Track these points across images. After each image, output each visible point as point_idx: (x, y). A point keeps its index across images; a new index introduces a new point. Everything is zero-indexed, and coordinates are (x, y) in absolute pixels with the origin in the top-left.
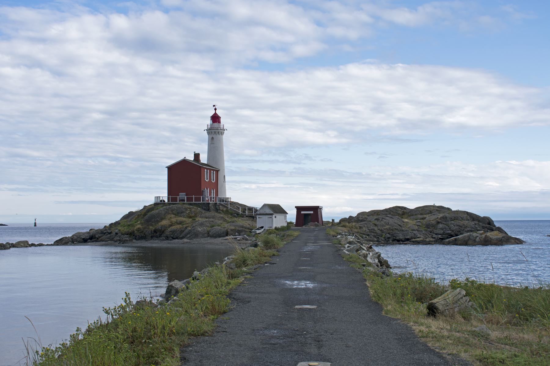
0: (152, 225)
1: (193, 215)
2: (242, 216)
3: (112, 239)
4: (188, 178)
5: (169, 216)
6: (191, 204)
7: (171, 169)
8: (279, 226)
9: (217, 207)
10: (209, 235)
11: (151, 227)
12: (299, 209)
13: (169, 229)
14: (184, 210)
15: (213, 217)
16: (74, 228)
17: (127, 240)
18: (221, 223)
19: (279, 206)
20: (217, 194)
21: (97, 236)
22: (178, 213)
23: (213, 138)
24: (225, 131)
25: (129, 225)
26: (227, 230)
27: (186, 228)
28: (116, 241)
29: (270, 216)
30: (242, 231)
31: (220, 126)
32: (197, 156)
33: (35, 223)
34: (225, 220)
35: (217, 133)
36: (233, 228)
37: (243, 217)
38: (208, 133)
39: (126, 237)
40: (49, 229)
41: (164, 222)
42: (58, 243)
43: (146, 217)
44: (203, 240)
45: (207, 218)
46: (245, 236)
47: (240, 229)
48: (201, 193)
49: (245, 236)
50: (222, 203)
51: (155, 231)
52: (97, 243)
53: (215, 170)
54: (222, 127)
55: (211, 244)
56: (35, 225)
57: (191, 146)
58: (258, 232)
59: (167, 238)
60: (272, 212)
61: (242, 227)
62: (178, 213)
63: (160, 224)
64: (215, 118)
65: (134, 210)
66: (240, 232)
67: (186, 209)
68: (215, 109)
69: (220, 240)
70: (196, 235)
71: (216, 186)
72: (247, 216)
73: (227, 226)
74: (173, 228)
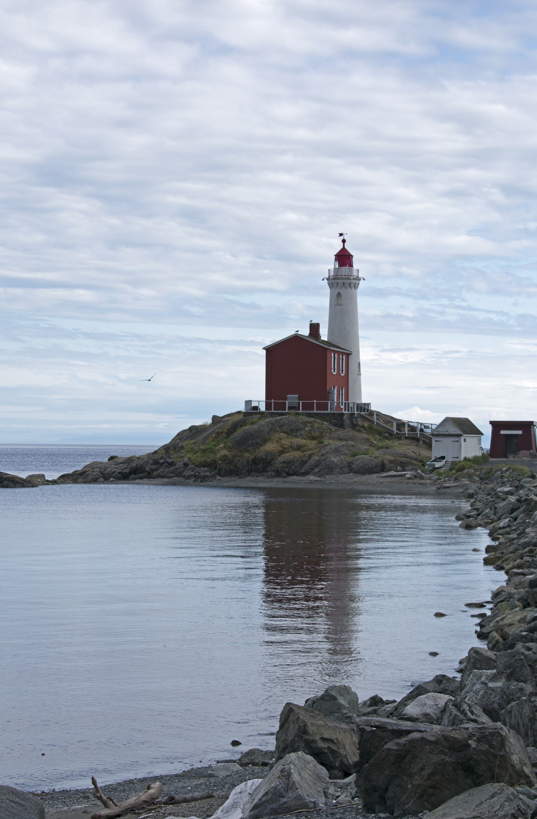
0: (248, 451)
1: (317, 434)
2: (399, 437)
3: (179, 475)
4: (305, 367)
5: (277, 436)
6: (310, 415)
8: (470, 455)
9: (354, 420)
10: (350, 469)
11: (246, 454)
12: (497, 426)
13: (281, 459)
14: (301, 426)
15: (352, 439)
16: (87, 455)
17: (208, 476)
18: (367, 450)
19: (467, 420)
20: (347, 399)
21: (147, 469)
22: (292, 431)
23: (339, 294)
24: (362, 282)
25: (204, 451)
26: (382, 461)
27: (310, 456)
28: (187, 478)
29: (456, 439)
30: (407, 464)
31: (351, 271)
32: (314, 328)
34: (372, 445)
35: (347, 285)
37: (399, 439)
38: (331, 285)
39: (204, 471)
40: (52, 455)
41: (270, 447)
42: (64, 479)
44: (342, 478)
45: (341, 440)
46: (419, 471)
47: (405, 460)
48: (326, 395)
49: (419, 471)
50: (363, 413)
51: (255, 461)
53: (347, 355)
54: (355, 274)
55: (362, 484)
57: (305, 311)
58: (437, 465)
59: (278, 474)
60: (459, 432)
61: (406, 456)
62: (293, 432)
63: (262, 448)
64: (344, 258)
65: (198, 422)
66: (404, 466)
67: (305, 424)
68: (344, 241)
70: (330, 469)
71: (346, 382)
72: (406, 438)
74: (287, 456)
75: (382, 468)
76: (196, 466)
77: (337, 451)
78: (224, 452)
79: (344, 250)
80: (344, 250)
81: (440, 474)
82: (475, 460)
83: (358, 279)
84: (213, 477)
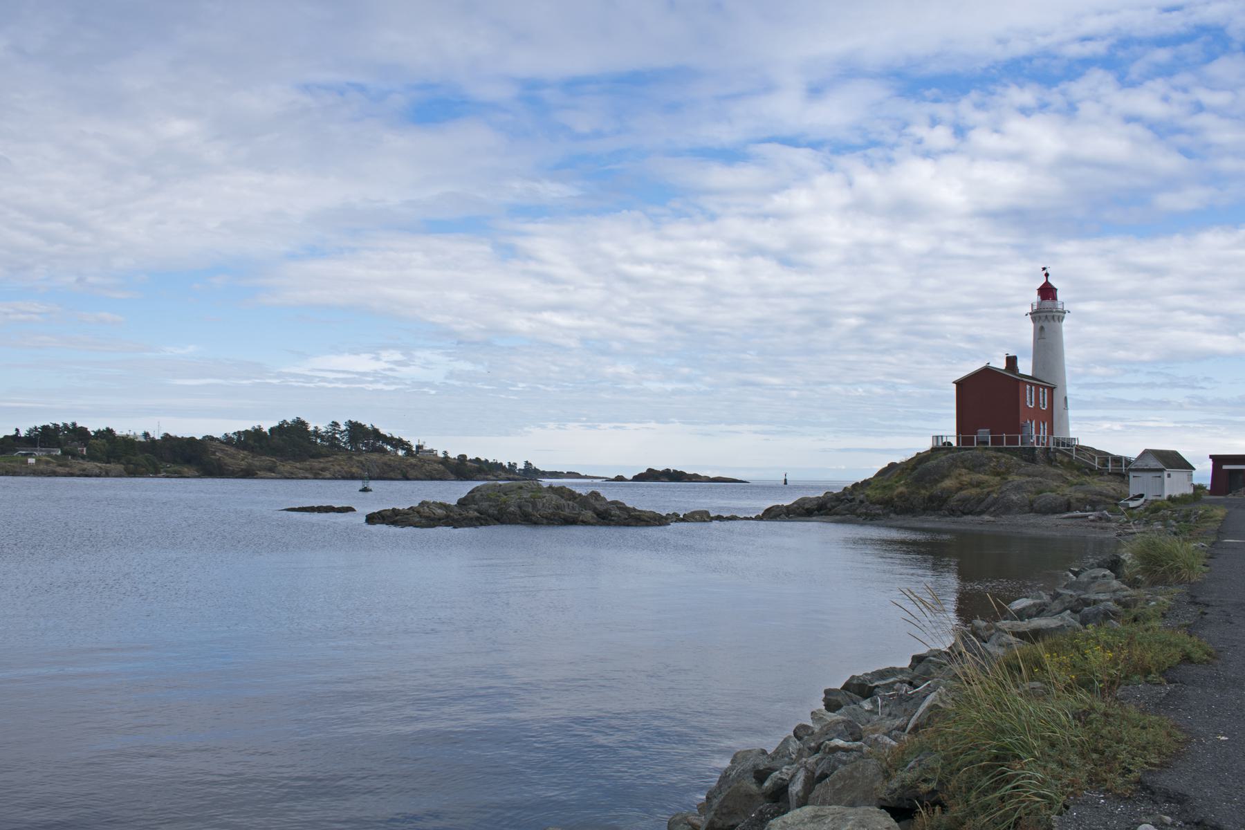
0: (924, 488)
2: (1100, 473)
3: (853, 512)
4: (997, 402)
5: (957, 471)
6: (999, 450)
7: (960, 384)
10: (1032, 508)
11: (923, 492)
12: (1218, 460)
13: (956, 497)
14: (986, 461)
15: (1042, 475)
20: (1051, 432)
23: (1042, 328)
27: (989, 494)
29: (1158, 474)
30: (1099, 502)
32: (1012, 361)
34: (1066, 481)
38: (1034, 320)
39: (878, 509)
41: (948, 483)
43: (915, 473)
44: (1020, 519)
51: (931, 498)
54: (1060, 307)
55: (1034, 526)
57: (1006, 340)
58: (1132, 504)
59: (952, 512)
61: (1100, 494)
62: (975, 467)
64: (1047, 292)
67: (990, 459)
68: (1047, 275)
69: (1053, 519)
70: (1007, 508)
71: (1048, 417)
74: (964, 493)
75: (1068, 507)
76: (871, 503)
77: (1018, 488)
79: (1047, 283)
80: (1047, 283)
81: (1132, 516)
82: (1184, 499)
84: (886, 515)
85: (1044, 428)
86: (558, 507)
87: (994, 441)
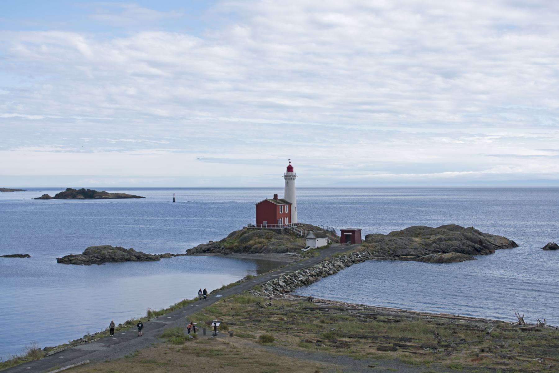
5: (254, 238)
6: (269, 230)
12: (343, 231)
13: (254, 247)
20: (290, 221)
30: (296, 249)
33: (174, 198)
34: (290, 241)
36: (292, 246)
38: (285, 179)
39: (228, 251)
41: (251, 242)
42: (190, 252)
43: (241, 238)
44: (272, 255)
48: (276, 222)
51: (246, 248)
52: (212, 254)
55: (274, 258)
56: (174, 201)
59: (252, 252)
62: (260, 236)
64: (290, 169)
67: (265, 233)
69: (282, 255)
70: (268, 251)
73: (290, 245)
74: (256, 246)
77: (273, 244)
78: (236, 244)
79: (290, 165)
80: (290, 165)
83: (295, 176)
85: (287, 219)
86: (123, 255)
87: (268, 226)
